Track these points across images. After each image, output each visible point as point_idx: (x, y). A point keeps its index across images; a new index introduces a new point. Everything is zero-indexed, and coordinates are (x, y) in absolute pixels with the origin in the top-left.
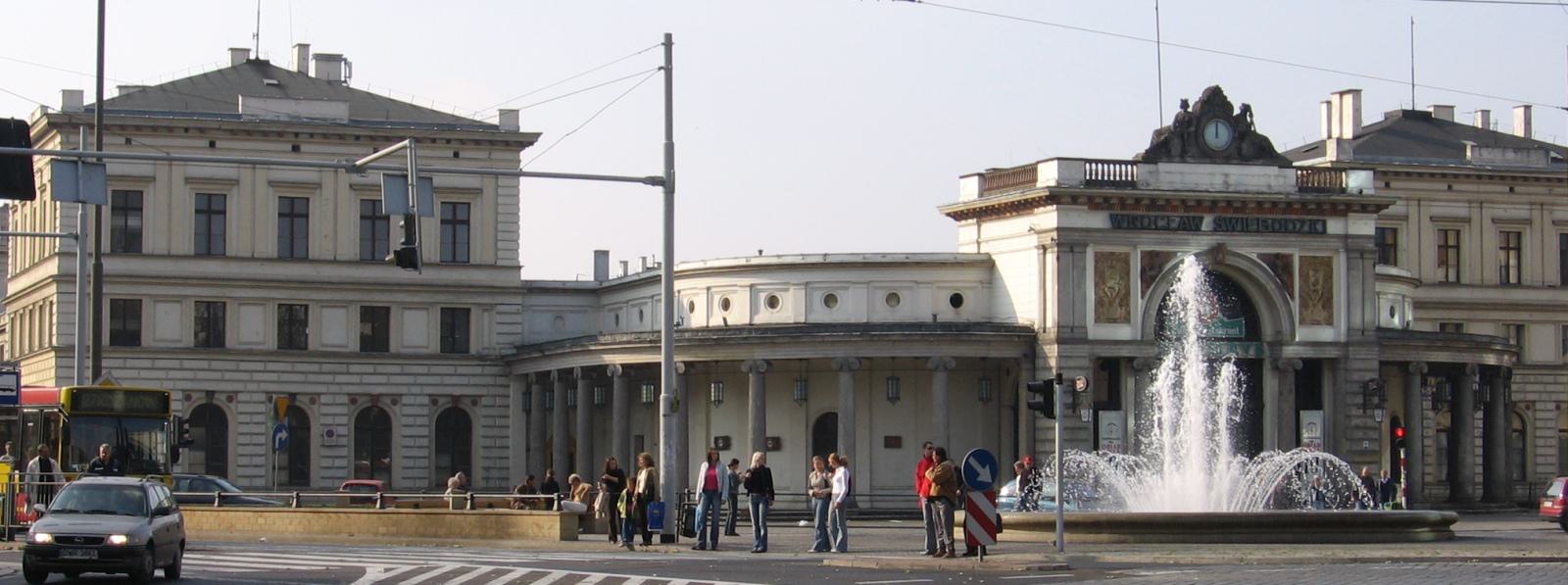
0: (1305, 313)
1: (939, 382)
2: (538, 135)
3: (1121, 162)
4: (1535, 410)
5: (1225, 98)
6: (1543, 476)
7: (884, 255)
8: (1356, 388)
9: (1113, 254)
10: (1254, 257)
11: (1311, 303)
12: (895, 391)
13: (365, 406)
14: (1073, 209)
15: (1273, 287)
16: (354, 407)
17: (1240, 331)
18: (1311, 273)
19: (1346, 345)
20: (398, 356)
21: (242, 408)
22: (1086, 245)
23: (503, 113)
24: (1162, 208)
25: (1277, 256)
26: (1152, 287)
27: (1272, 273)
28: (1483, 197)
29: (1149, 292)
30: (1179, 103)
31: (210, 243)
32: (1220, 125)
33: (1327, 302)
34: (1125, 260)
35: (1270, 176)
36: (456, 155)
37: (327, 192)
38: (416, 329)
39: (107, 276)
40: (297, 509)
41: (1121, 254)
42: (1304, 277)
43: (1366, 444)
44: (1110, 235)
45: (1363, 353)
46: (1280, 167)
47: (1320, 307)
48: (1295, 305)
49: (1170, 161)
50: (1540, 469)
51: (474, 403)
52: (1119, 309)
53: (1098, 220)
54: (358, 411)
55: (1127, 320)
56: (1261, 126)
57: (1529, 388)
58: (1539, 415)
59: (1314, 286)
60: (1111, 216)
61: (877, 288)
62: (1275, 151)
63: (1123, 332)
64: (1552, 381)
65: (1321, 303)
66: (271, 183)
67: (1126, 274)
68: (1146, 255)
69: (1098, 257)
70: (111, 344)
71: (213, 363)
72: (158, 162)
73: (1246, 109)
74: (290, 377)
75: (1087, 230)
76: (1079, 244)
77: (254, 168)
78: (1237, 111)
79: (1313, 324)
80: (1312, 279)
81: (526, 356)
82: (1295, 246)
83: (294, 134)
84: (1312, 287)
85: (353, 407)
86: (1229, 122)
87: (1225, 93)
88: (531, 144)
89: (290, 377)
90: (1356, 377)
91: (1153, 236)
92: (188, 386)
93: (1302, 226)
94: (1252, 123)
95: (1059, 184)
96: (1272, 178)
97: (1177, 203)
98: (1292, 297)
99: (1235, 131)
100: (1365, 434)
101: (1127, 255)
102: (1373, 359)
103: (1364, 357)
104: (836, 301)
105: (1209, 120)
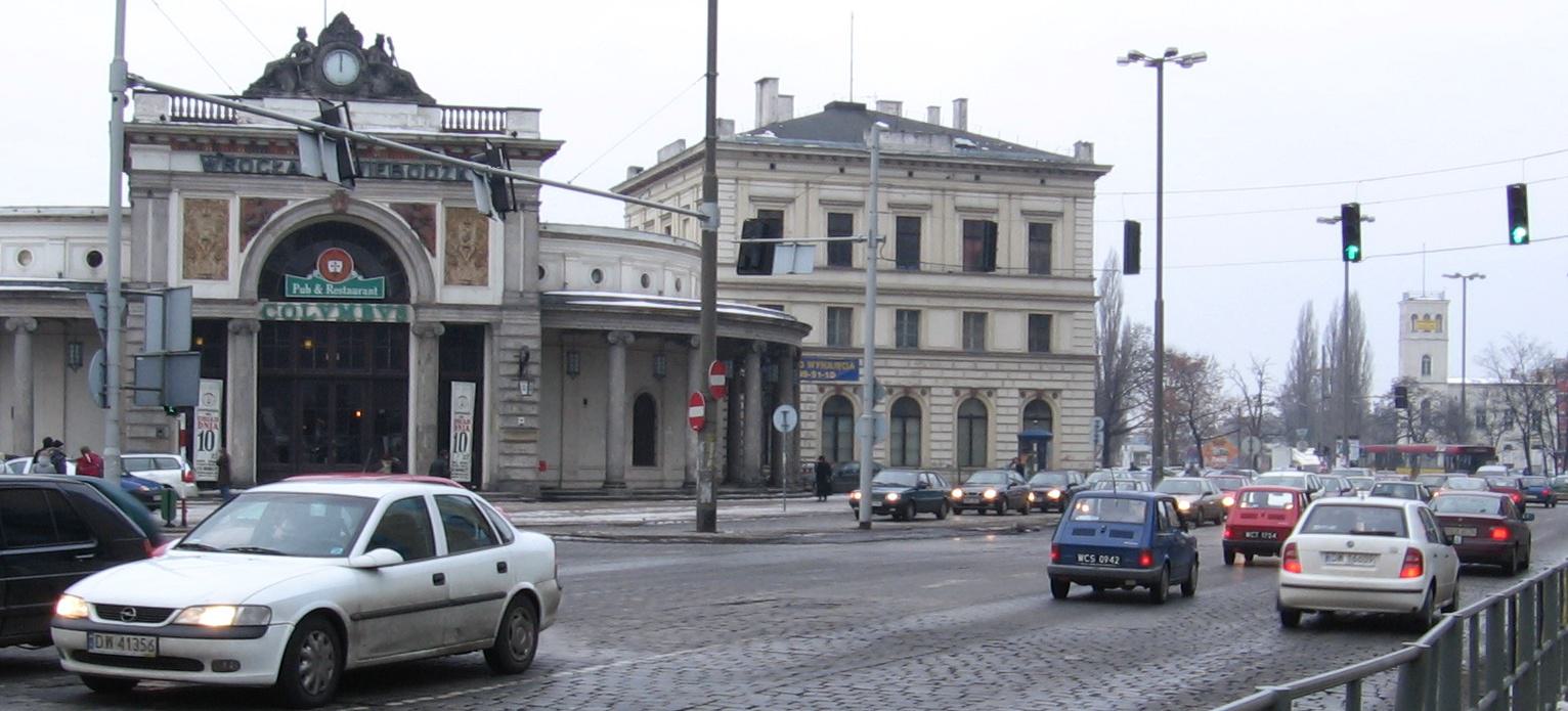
0: (453, 273)
1: (618, 357)
2: (1109, 168)
3: (197, 97)
4: (932, 396)
5: (352, 26)
6: (937, 462)
7: (15, 209)
8: (510, 357)
9: (207, 201)
10: (386, 207)
11: (199, 254)
12: (77, 357)
13: (899, 396)
14: (151, 150)
15: (409, 241)
16: (822, 395)
17: (379, 292)
18: (461, 226)
19: (501, 308)
20: (1056, 357)
21: (935, 400)
22: (169, 191)
23: (1078, 145)
24: (265, 149)
25: (415, 206)
26: (253, 240)
27: (409, 227)
28: (1078, 192)
29: (250, 244)
30: (296, 31)
31: (840, 256)
32: (344, 56)
33: (481, 259)
34: (224, 209)
35: (406, 115)
36: (842, 170)
37: (937, 211)
38: (1008, 332)
39: (720, 283)
40: (415, 478)
41: (218, 201)
42: (450, 229)
43: (521, 421)
44: (202, 179)
45: (520, 317)
46: (420, 106)
47: (472, 265)
48: (438, 264)
49: (278, 96)
50: (935, 455)
51: (1055, 396)
52: (214, 263)
53: (190, 163)
54: (1026, 404)
55: (224, 276)
56: (404, 61)
57: (925, 373)
58: (1001, 402)
59: (465, 241)
60: (202, 157)
61: (74, 245)
62: (416, 88)
63: (227, 289)
64: (950, 367)
65: (473, 261)
66: (957, 209)
67: (223, 224)
68: (247, 204)
69: (189, 205)
70: (720, 339)
71: (956, 363)
72: (1001, 196)
73: (380, 39)
74: (970, 375)
75: (172, 174)
76: (159, 190)
77: (1010, 199)
78: (368, 43)
79: (463, 284)
80: (462, 234)
81: (1353, 365)
82: (436, 195)
83: (910, 164)
84: (462, 243)
85: (1022, 400)
86: (358, 56)
87: (352, 21)
88: (1103, 174)
89: (970, 375)
90: (511, 344)
91: (256, 182)
92: (961, 383)
93: (447, 173)
94: (393, 57)
95: (1094, 180)
96: (410, 118)
97: (205, 141)
98: (434, 255)
99: (362, 63)
100: (521, 409)
101: (226, 202)
102: (534, 325)
103: (523, 322)
104: (31, 258)
105: (330, 51)
